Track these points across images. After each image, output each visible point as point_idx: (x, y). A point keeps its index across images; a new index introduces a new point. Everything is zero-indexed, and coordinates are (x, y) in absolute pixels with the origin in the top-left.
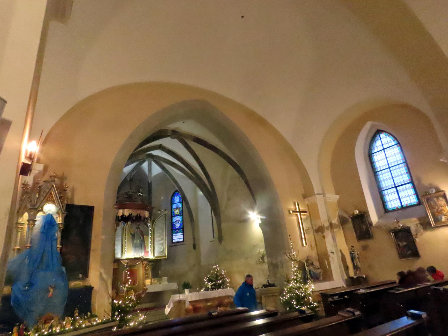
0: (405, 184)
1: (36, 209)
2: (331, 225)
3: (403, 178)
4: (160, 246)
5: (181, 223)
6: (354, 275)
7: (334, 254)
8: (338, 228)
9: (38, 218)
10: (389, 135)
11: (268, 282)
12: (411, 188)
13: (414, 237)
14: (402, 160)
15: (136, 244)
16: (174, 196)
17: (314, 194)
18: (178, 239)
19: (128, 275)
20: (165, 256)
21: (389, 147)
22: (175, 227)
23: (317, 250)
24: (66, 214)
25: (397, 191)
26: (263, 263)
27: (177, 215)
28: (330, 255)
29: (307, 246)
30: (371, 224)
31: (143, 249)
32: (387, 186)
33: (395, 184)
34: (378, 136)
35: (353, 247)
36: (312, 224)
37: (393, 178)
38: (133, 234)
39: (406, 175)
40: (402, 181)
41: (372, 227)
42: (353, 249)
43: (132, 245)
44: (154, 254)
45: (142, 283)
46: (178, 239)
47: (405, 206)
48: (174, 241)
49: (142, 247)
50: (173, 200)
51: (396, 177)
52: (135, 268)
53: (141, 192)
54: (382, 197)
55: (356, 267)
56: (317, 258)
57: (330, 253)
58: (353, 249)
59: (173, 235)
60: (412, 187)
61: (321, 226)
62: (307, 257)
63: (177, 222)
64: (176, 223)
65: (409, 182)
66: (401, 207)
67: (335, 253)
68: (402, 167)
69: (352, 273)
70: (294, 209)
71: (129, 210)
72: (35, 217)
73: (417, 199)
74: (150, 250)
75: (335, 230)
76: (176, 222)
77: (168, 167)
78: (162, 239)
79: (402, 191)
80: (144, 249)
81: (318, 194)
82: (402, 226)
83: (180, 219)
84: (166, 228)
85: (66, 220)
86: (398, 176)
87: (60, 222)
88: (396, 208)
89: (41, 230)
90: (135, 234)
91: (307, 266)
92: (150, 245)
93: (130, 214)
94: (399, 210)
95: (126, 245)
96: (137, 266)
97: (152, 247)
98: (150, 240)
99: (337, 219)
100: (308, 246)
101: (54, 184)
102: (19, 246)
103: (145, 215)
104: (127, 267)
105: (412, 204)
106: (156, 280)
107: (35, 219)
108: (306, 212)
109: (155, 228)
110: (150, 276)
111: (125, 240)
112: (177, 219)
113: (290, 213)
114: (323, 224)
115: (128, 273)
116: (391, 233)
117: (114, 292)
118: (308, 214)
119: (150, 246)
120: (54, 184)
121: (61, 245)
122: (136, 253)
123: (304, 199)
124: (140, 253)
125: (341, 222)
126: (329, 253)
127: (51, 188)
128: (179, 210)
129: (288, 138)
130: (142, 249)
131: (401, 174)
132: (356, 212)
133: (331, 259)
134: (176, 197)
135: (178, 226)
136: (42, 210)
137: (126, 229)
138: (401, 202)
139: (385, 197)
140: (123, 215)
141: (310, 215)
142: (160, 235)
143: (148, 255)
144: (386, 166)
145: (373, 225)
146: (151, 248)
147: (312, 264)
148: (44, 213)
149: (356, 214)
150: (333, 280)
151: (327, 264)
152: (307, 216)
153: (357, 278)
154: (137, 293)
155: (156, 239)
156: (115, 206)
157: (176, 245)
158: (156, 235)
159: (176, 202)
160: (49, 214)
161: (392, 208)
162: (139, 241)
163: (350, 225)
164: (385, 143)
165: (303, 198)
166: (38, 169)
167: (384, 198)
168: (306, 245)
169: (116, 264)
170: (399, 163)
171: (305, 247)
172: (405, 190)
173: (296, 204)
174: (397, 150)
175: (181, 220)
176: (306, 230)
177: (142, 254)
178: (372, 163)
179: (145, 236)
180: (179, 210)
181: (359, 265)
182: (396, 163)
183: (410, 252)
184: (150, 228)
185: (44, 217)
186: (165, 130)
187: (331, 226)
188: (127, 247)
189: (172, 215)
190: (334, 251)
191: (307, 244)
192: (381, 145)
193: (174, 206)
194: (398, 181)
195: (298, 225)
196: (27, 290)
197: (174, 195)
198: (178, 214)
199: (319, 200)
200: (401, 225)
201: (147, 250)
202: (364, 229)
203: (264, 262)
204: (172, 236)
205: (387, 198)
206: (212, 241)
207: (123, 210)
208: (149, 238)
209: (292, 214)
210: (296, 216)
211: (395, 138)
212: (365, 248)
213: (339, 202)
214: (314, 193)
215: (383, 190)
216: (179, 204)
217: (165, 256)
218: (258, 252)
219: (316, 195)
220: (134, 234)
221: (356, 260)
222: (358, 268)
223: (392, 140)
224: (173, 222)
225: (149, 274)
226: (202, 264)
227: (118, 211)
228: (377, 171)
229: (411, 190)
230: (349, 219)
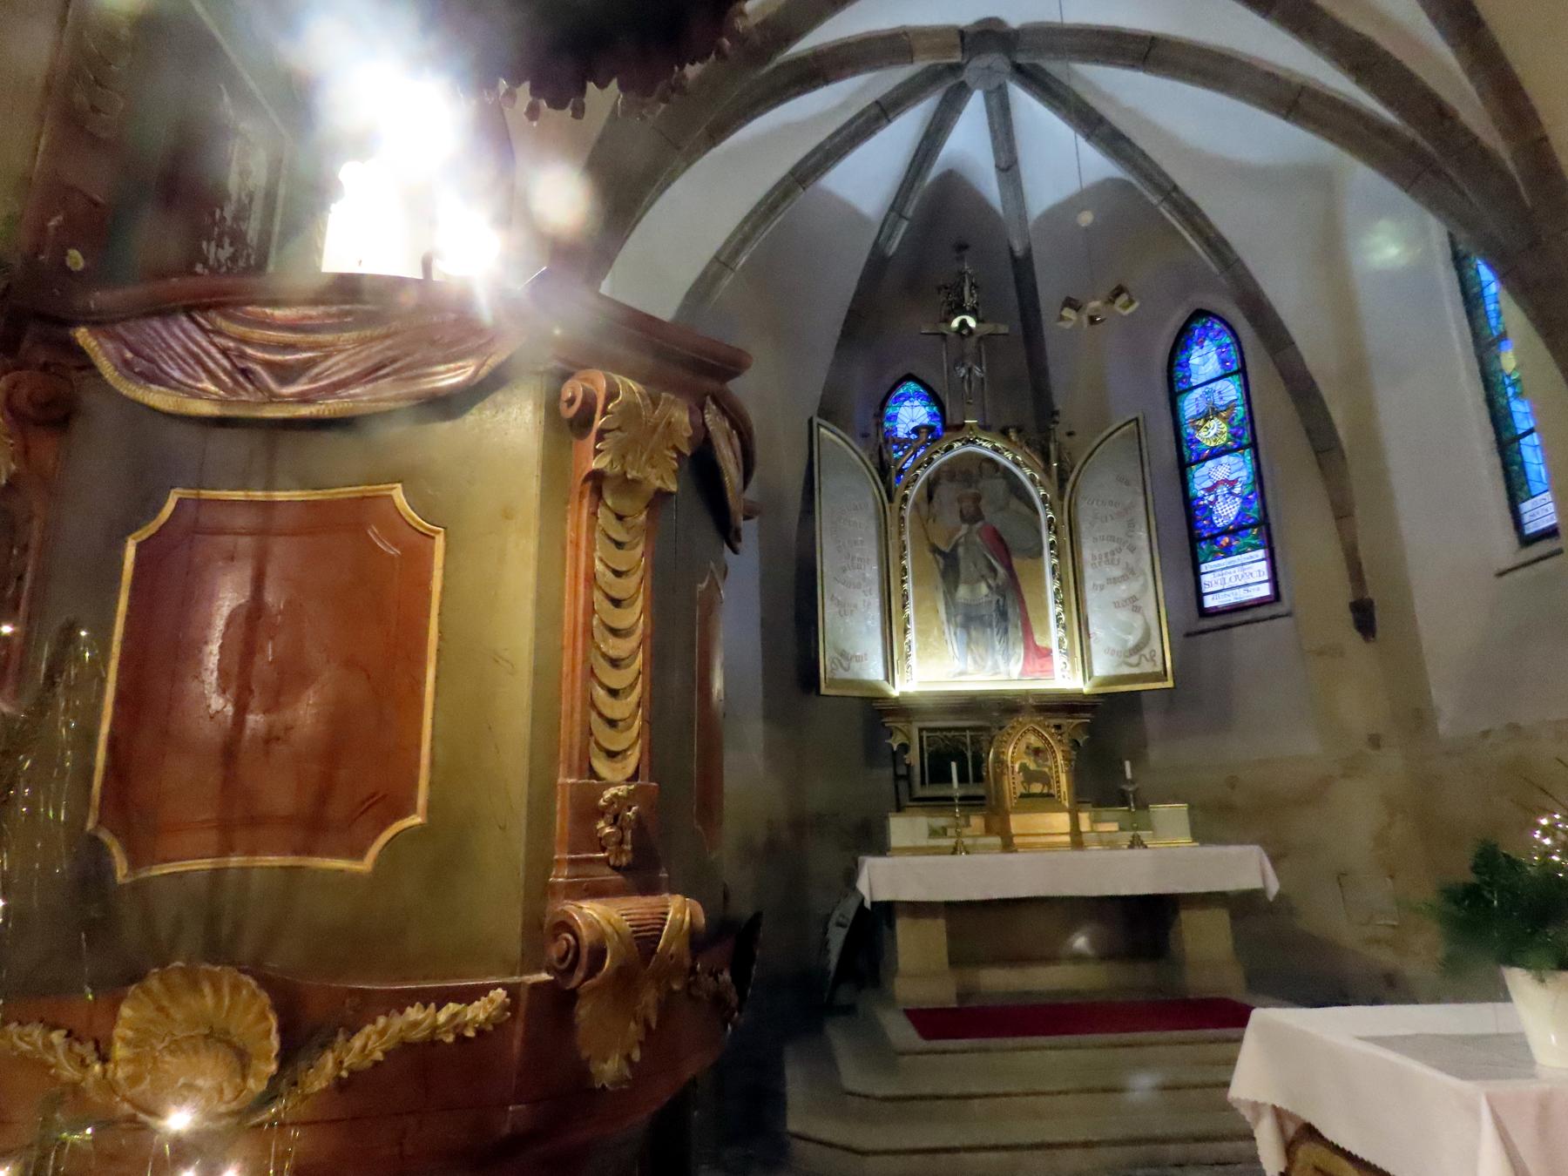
4: (1124, 615)
5: (1246, 492)
15: (967, 606)
16: (1186, 348)
18: (1240, 587)
20: (1162, 676)
22: (1212, 521)
27: (1216, 453)
31: (1016, 634)
46: (1240, 587)
48: (1210, 602)
59: (1204, 568)
64: (1211, 498)
74: (1061, 641)
76: (1210, 490)
78: (1130, 573)
83: (1240, 470)
84: (1153, 523)
90: (961, 550)
92: (1053, 609)
95: (910, 611)
97: (1071, 624)
110: (1064, 788)
111: (903, 582)
119: (1058, 620)
122: (975, 662)
134: (1197, 348)
135: (1226, 511)
143: (1048, 672)
146: (1064, 628)
155: (1091, 576)
162: (984, 589)
177: (1013, 661)
180: (1229, 421)
184: (1045, 515)
188: (917, 623)
189: (1186, 458)
193: (1191, 405)
197: (1182, 341)
198: (1222, 440)
201: (1039, 640)
204: (1197, 574)
208: (1048, 571)
220: (955, 549)
224: (1192, 493)
226: (1443, 727)
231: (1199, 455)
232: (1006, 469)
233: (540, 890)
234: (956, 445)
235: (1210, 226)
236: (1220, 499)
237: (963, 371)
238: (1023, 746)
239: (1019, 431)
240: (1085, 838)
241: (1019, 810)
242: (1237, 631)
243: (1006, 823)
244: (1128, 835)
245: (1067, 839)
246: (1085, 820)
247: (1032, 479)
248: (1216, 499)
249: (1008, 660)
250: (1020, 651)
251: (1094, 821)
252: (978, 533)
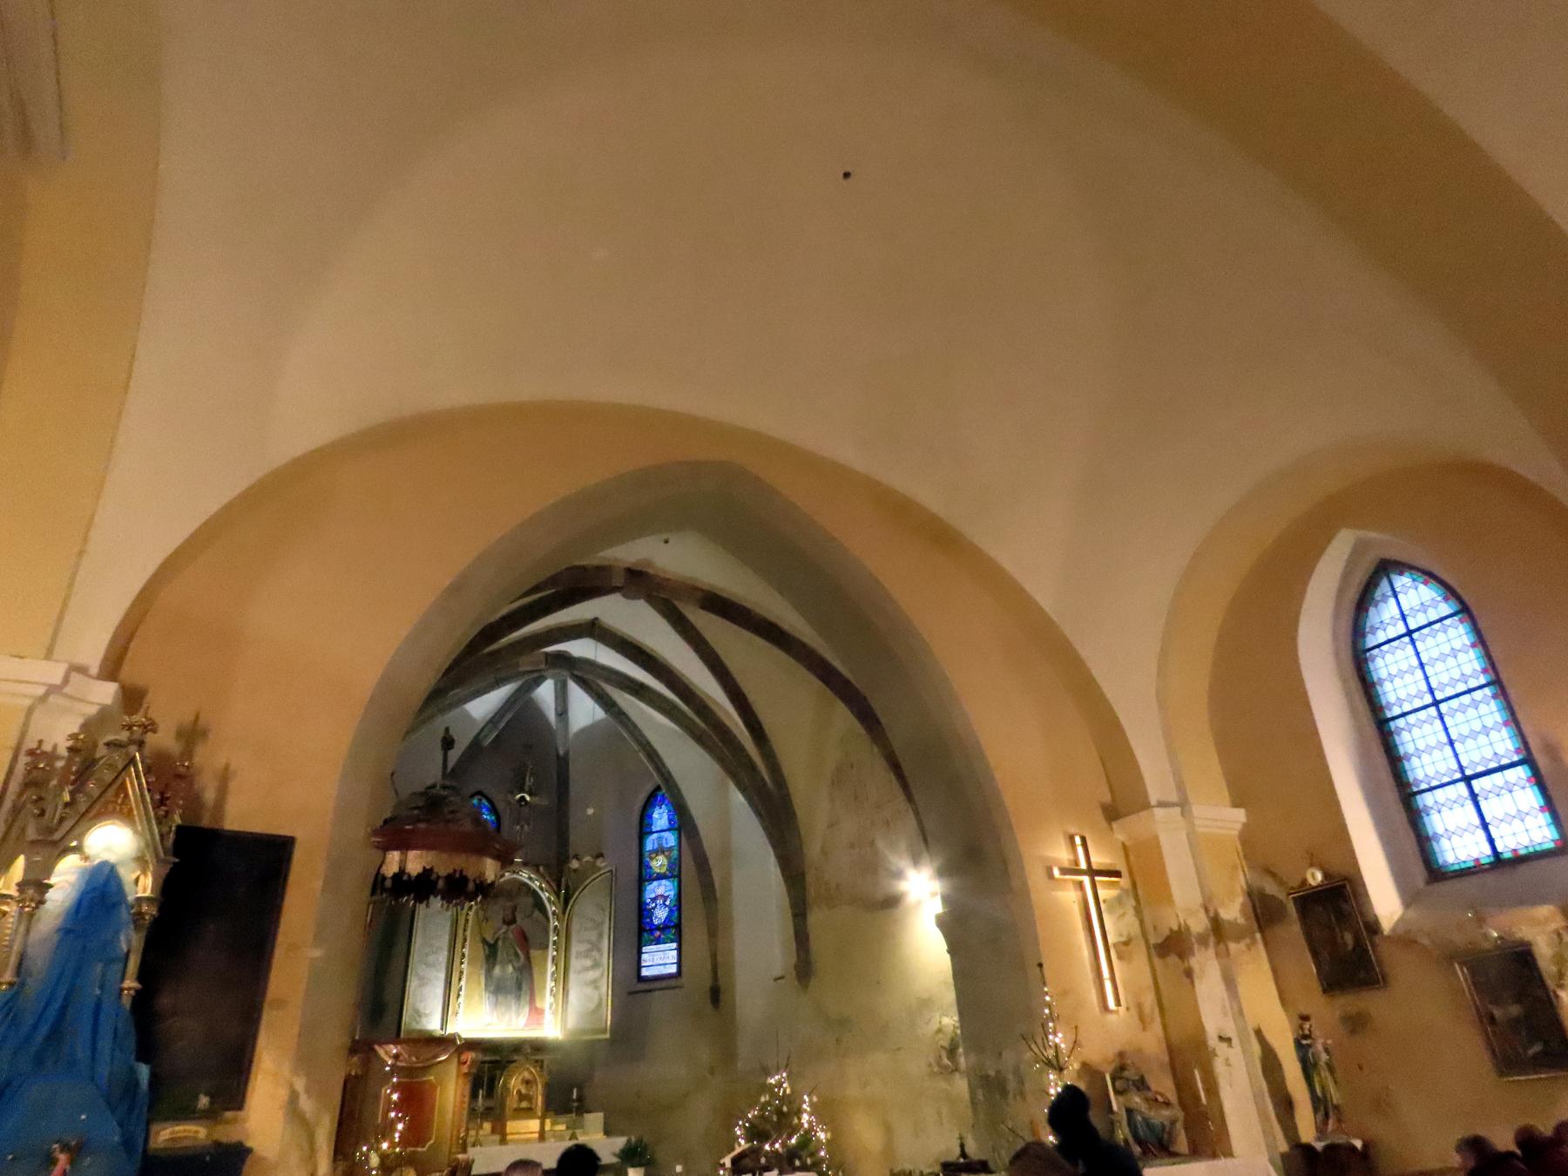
0: (1501, 768)
1: (55, 844)
2: (1217, 926)
3: (1491, 744)
4: (589, 990)
6: (1319, 1139)
7: (1230, 1045)
8: (1248, 941)
9: (60, 875)
10: (1426, 577)
11: (963, 1154)
12: (1528, 785)
13: (1550, 983)
14: (1485, 671)
17: (1145, 805)
19: (395, 1103)
20: (604, 1031)
21: (1430, 624)
22: (652, 920)
23: (1165, 1026)
24: (175, 864)
25: (1474, 797)
26: (953, 1071)
27: (660, 877)
28: (1218, 1052)
29: (1122, 1009)
30: (1373, 927)
32: (1431, 774)
33: (1461, 768)
34: (1384, 584)
35: (1305, 1018)
36: (1142, 922)
37: (1451, 743)
38: (492, 942)
39: (1505, 732)
40: (1489, 755)
41: (1377, 939)
42: (1307, 1026)
43: (486, 985)
44: (564, 1020)
45: (452, 1136)
47: (1508, 855)
48: (645, 972)
49: (523, 993)
50: (646, 822)
51: (1463, 738)
52: (425, 1079)
53: (527, 789)
54: (1414, 817)
55: (1320, 1104)
56: (1166, 1058)
57: (1217, 1040)
58: (1307, 1026)
59: (644, 949)
60: (1533, 780)
61: (1176, 932)
62: (1121, 1055)
63: (660, 901)
64: (654, 905)
65: (1516, 758)
66: (1492, 859)
67: (1235, 1041)
68: (1484, 701)
69: (1307, 1132)
70: (1069, 860)
71: (424, 852)
72: (49, 871)
73: (1553, 828)
74: (551, 1005)
75: (1232, 946)
76: (654, 900)
77: (625, 700)
78: (596, 965)
79: (1491, 795)
80: (528, 999)
81: (1161, 804)
82: (1496, 939)
85: (169, 888)
86: (1474, 735)
87: (144, 891)
88: (1472, 864)
89: (65, 921)
90: (500, 943)
91: (1117, 1092)
92: (550, 984)
93: (428, 867)
94: (1486, 871)
95: (463, 983)
96: (435, 1070)
98: (550, 968)
99: (1242, 905)
100: (1128, 1009)
101: (137, 755)
103: (482, 874)
104: (392, 1073)
105: (1538, 848)
106: (563, 1123)
107: (46, 881)
108: (1117, 874)
109: (574, 923)
112: (661, 889)
113: (1051, 876)
114: (1185, 922)
115: (395, 1097)
116: (1457, 966)
118: (1124, 881)
119: (552, 990)
120: (137, 755)
123: (1110, 824)
124: (513, 1016)
125: (1256, 915)
126: (1213, 1042)
127: (126, 767)
128: (666, 857)
129: (1045, 595)
130: (522, 1002)
131: (1484, 726)
132: (1313, 876)
133: (1219, 1066)
134: (657, 808)
135: (660, 915)
136: (78, 849)
137: (467, 920)
138: (1491, 841)
139: (1426, 819)
140: (402, 871)
141: (1134, 884)
142: (588, 950)
143: (539, 1023)
144: (1422, 699)
145: (1382, 933)
146: (554, 996)
147: (1141, 1085)
148: (86, 858)
149: (1313, 883)
150: (1229, 1154)
151: (1200, 1085)
152: (1122, 889)
153: (1328, 1148)
155: (575, 964)
156: (373, 839)
157: (650, 991)
158: (576, 948)
159: (658, 829)
160: (104, 864)
161: (1458, 863)
162: (510, 969)
163: (1292, 930)
164: (1411, 609)
165: (1106, 819)
166: (97, 700)
167: (1424, 824)
168: (1118, 1003)
170: (1473, 683)
171: (1117, 1012)
172: (1503, 791)
173: (1078, 840)
174: (1458, 634)
175: (672, 893)
176: (1115, 945)
177: (521, 1018)
178: (1366, 686)
179: (534, 953)
180: (668, 858)
181: (1335, 1096)
182: (1461, 688)
183: (1537, 1048)
184: (554, 923)
185: (84, 871)
186: (600, 569)
187: (1218, 929)
189: (644, 876)
190: (1231, 1032)
191: (1123, 1001)
192: (1399, 616)
193: (650, 843)
194: (1475, 755)
195: (1083, 923)
198: (663, 870)
199: (1167, 829)
200: (1496, 935)
201: (538, 1004)
202: (1350, 947)
203: (957, 1070)
204: (640, 953)
205: (1436, 823)
206: (780, 978)
207: (402, 853)
208: (549, 974)
209: (1057, 880)
210: (1076, 889)
211: (1450, 592)
212: (1356, 1024)
213: (1247, 839)
214: (1146, 796)
215: (1415, 789)
216: (666, 834)
217: (604, 1031)
218: (934, 1026)
219: (1153, 807)
221: (1319, 1075)
222: (1330, 1106)
223: (1439, 599)
225: (537, 1097)
227: (384, 858)
228: (1389, 715)
229: (1529, 790)
230: (1285, 902)
231: (650, 877)
232: (534, 890)
233: (450, 1152)
234: (507, 874)
235: (663, 764)
237: (518, 827)
238: (521, 1078)
239: (546, 866)
240: (546, 1136)
241: (515, 1118)
242: (657, 994)
243: (504, 1126)
244: (570, 1132)
245: (537, 1135)
246: (548, 1122)
247: (549, 899)
248: (656, 905)
249: (518, 1015)
250: (526, 1009)
251: (553, 1124)
252: (512, 932)
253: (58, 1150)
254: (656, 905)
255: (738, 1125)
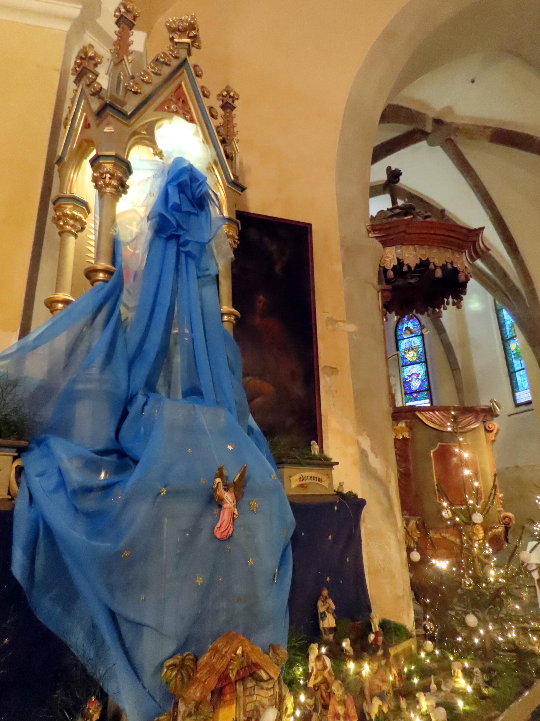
5: (423, 378)
22: (410, 388)
27: (412, 363)
63: (414, 377)
64: (410, 379)
76: (410, 376)
83: (421, 370)
102: (72, 294)
117: (412, 523)
121: (235, 304)
128: (415, 351)
154: (490, 533)
169: (402, 425)
180: (417, 352)
193: (403, 345)
196: (107, 488)
198: (414, 359)
236: (413, 380)
248: (412, 379)
253: (221, 486)
254: (412, 379)
255: (443, 508)
